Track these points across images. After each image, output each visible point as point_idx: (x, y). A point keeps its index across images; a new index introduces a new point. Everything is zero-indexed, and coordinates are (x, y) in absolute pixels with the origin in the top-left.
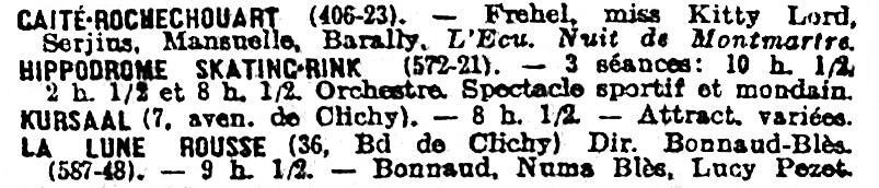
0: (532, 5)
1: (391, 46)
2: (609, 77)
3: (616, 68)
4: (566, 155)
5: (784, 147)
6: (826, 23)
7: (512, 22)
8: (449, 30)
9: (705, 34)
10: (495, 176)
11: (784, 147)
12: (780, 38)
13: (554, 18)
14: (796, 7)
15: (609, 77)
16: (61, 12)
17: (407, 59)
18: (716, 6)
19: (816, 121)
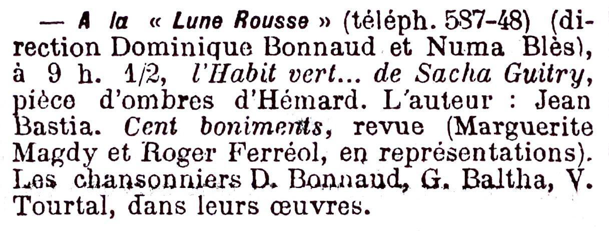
0: (416, 12)
1: (520, 187)
2: (478, 89)
3: (556, 51)
4: (443, 115)
5: (588, 23)
6: (181, 107)
7: (67, 55)
8: (339, 108)
9: (24, 148)
10: (367, 212)
11: (588, 23)
12: (270, 124)
13: (543, 131)
14: (14, 55)
15: (478, 89)
16: (19, 161)
17: (455, 150)
18: (64, 38)
19: (556, 51)
